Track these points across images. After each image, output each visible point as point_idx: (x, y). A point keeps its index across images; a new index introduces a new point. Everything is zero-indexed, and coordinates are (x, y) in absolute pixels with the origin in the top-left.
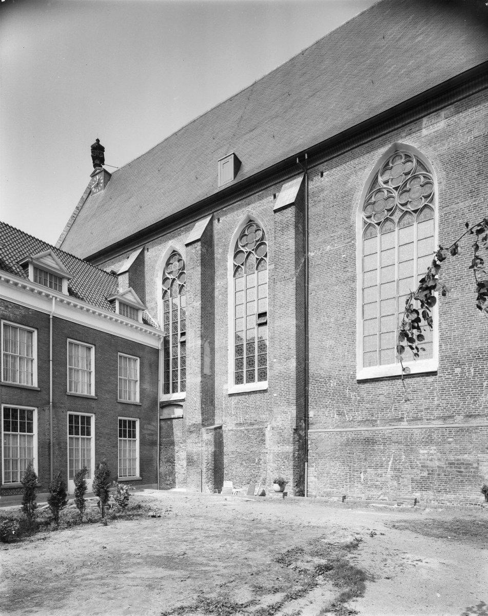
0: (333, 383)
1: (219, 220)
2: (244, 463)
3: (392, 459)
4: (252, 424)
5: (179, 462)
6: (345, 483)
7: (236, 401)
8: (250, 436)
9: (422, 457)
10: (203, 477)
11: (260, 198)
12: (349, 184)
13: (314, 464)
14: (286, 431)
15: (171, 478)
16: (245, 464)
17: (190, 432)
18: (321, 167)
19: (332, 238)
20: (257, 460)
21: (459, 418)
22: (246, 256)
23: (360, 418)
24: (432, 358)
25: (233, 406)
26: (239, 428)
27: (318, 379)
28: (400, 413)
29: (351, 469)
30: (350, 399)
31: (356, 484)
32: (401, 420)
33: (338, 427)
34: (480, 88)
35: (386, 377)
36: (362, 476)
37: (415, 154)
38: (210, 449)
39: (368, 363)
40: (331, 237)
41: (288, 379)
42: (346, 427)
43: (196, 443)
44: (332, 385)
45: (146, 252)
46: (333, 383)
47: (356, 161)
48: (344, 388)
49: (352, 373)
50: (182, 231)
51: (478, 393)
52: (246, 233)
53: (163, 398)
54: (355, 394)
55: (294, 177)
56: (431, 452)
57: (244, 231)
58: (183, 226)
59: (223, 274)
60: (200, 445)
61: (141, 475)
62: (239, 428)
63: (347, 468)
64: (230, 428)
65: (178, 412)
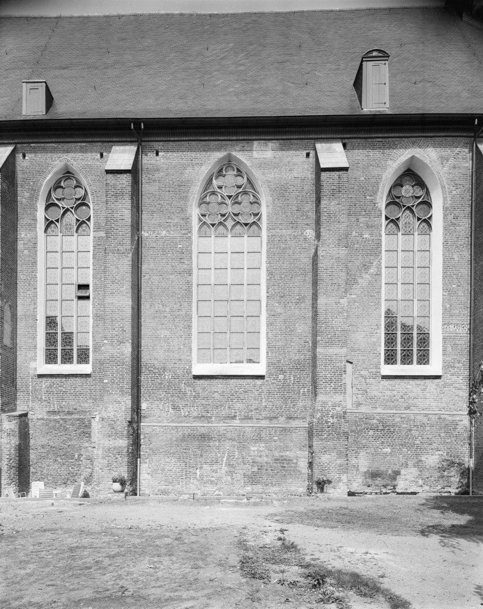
0: (168, 376)
1: (24, 156)
2: (59, 459)
3: (226, 455)
4: (69, 413)
7: (48, 384)
11: (83, 150)
13: (147, 461)
14: (119, 423)
18: (157, 146)
20: (76, 456)
21: (282, 419)
23: (195, 414)
29: (188, 465)
30: (185, 393)
32: (234, 417)
33: (173, 421)
35: (222, 376)
36: (198, 472)
38: (13, 442)
40: (167, 223)
42: (181, 422)
44: (167, 377)
45: (19, 156)
47: (193, 154)
49: (187, 367)
52: (62, 184)
56: (260, 449)
59: (30, 225)
64: (40, 417)
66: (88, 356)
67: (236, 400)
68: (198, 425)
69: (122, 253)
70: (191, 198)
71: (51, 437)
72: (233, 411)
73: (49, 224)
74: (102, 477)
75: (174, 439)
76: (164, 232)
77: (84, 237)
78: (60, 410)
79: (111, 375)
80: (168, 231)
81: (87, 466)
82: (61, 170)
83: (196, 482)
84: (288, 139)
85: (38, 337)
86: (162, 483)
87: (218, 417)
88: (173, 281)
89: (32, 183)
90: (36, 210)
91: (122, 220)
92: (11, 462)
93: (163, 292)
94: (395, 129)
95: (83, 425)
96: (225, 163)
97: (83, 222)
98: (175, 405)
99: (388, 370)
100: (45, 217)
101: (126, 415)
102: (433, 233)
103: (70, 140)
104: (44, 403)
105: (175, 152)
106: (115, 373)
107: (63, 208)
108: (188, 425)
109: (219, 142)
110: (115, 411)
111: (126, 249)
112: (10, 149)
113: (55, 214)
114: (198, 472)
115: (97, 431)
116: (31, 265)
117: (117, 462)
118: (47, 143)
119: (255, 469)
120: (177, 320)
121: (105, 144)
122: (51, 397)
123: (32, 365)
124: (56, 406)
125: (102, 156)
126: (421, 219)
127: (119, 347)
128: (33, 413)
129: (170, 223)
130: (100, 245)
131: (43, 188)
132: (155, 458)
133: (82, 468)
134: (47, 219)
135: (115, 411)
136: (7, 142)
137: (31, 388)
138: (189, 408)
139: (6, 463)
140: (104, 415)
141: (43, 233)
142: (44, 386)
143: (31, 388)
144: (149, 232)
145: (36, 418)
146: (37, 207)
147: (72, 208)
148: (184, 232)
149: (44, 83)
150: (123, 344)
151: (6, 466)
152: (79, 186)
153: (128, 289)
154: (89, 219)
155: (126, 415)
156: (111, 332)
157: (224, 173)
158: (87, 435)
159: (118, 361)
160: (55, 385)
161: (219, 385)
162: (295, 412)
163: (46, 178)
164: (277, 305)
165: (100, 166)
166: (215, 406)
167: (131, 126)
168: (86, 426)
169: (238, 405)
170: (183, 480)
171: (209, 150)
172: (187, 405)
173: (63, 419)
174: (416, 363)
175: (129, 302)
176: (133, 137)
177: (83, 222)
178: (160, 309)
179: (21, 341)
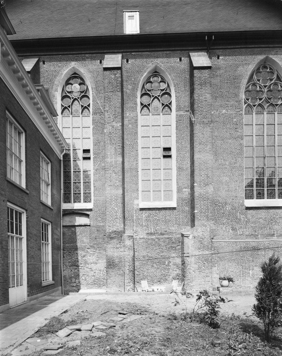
0: (228, 208)
1: (127, 61)
2: (155, 265)
4: (162, 234)
5: (87, 265)
6: (239, 278)
7: (147, 215)
8: (161, 243)
10: (126, 278)
11: (168, 56)
12: (239, 72)
13: (216, 265)
14: (205, 239)
15: (77, 281)
17: (111, 238)
18: (218, 52)
19: (227, 105)
20: (167, 263)
22: (152, 99)
23: (247, 233)
24: (172, 200)
25: (144, 219)
26: (150, 237)
27: (217, 203)
28: (272, 231)
29: (244, 268)
30: (240, 220)
31: (247, 278)
32: (273, 235)
33: (232, 238)
36: (251, 272)
37: (276, 69)
39: (145, 199)
40: (226, 104)
41: (207, 200)
42: (238, 239)
43: (117, 248)
44: (227, 209)
45: (41, 63)
46: (228, 208)
47: (243, 57)
48: (236, 212)
49: (241, 202)
50: (88, 58)
51: (167, 222)
52: (151, 80)
53: (65, 206)
54: (243, 216)
57: (149, 78)
58: (89, 53)
59: (132, 107)
60: (122, 250)
61: (53, 279)
62: (150, 237)
63: (241, 267)
64: (142, 237)
65: (80, 220)
67: (274, 223)
68: (249, 240)
69: (206, 124)
70: (242, 87)
71: (149, 251)
72: (272, 231)
73: (64, 109)
77: (167, 116)
79: (199, 207)
80: (227, 110)
81: (174, 270)
83: (249, 279)
85: (139, 183)
87: (262, 235)
88: (230, 144)
89: (133, 79)
90: (137, 98)
91: (206, 101)
92: (130, 268)
93: (224, 151)
95: (171, 242)
96: (262, 64)
97: (86, 107)
98: (234, 227)
99: (249, 203)
100: (62, 104)
102: (172, 113)
104: (144, 228)
105: (230, 56)
106: (202, 206)
107: (73, 98)
109: (261, 49)
110: (203, 232)
111: (209, 121)
112: (36, 59)
113: (68, 102)
114: (251, 272)
116: (133, 135)
117: (204, 266)
121: (183, 52)
122: (149, 223)
123: (136, 202)
124: (152, 229)
125: (180, 60)
126: (70, 105)
128: (137, 234)
129: (228, 104)
130: (181, 120)
131: (141, 82)
132: (221, 263)
133: (171, 271)
134: (62, 106)
135: (203, 232)
136: (116, 51)
137: (135, 218)
138: (243, 229)
139: (127, 268)
140: (196, 234)
141: (61, 115)
142: (144, 216)
144: (214, 111)
145: (139, 238)
146: (137, 95)
147: (78, 98)
148: (237, 110)
149: (138, 12)
150: (208, 186)
151: (127, 271)
152: (163, 81)
153: (210, 148)
154: (89, 105)
155: (211, 234)
156: (199, 178)
157: (261, 70)
158: (174, 249)
159: (205, 198)
160: (151, 215)
161: (263, 213)
163: (143, 76)
165: (180, 67)
166: (260, 228)
167: (206, 37)
170: (241, 278)
171: (254, 54)
172: (241, 227)
174: (171, 202)
177: (66, 108)
178: (222, 163)
179: (127, 186)
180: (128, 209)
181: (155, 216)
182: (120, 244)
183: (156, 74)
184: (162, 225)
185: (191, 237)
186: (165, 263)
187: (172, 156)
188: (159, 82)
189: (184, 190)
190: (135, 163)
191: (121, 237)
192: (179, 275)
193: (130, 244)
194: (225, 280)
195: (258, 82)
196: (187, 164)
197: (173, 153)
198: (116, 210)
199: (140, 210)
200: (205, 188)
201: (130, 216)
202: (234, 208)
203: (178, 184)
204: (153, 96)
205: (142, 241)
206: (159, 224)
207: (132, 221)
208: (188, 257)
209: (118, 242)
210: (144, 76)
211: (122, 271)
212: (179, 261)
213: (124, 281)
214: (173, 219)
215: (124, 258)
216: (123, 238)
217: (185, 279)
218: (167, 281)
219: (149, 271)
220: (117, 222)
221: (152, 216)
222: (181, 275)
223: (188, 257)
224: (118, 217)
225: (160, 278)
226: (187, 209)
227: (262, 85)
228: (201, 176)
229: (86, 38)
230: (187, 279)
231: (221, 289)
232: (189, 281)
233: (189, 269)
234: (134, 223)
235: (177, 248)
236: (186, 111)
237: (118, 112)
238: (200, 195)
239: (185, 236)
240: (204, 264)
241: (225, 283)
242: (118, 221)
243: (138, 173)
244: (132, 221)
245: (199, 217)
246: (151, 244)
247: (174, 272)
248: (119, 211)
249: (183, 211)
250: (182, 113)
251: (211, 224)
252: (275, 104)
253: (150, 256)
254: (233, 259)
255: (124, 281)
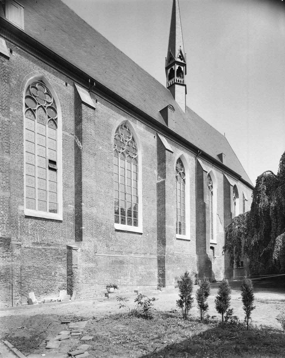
0: (104, 228)
3: (130, 271)
4: (48, 245)
8: (47, 254)
9: (140, 270)
14: (91, 253)
16: (42, 277)
20: (53, 274)
21: (148, 254)
23: (116, 250)
26: (36, 247)
29: (115, 277)
30: (111, 239)
33: (106, 253)
34: (26, 49)
35: (127, 231)
39: (31, 206)
41: (92, 220)
44: (103, 229)
47: (113, 112)
51: (54, 233)
55: (79, 85)
56: (142, 268)
57: (35, 83)
60: (10, 259)
62: (36, 247)
66: (39, 206)
69: (91, 154)
74: (82, 286)
75: (108, 263)
76: (101, 148)
78: (42, 242)
80: (103, 147)
81: (60, 280)
82: (39, 78)
84: (148, 126)
86: (103, 287)
92: (19, 279)
94: (67, 72)
95: (58, 253)
101: (95, 249)
102: (58, 130)
103: (125, 111)
104: (30, 237)
108: (114, 255)
115: (79, 258)
118: (30, 53)
119: (141, 278)
120: (107, 198)
122: (35, 233)
123: (20, 208)
125: (66, 84)
127: (90, 209)
137: (19, 224)
139: (16, 280)
142: (30, 224)
143: (19, 224)
151: (16, 282)
152: (48, 93)
160: (38, 225)
162: (152, 251)
164: (146, 201)
168: (59, 254)
169: (133, 247)
173: (44, 249)
175: (85, 182)
176: (88, 86)
180: (11, 214)
181: (42, 226)
182: (7, 253)
183: (42, 84)
184: (48, 236)
185: (79, 251)
186: (52, 273)
187: (58, 171)
188: (45, 93)
189: (69, 206)
190: (19, 166)
191: (9, 245)
192: (64, 285)
193: (19, 253)
194: (112, 287)
195: (122, 136)
196: (72, 182)
197: (59, 166)
198: (2, 214)
199: (25, 218)
200: (90, 209)
201: (13, 222)
202: (107, 229)
203: (64, 199)
204: (39, 104)
205: (27, 250)
206: (45, 234)
207: (15, 228)
208: (76, 268)
209: (5, 250)
210: (31, 79)
211: (10, 283)
212: (64, 271)
213: (12, 294)
214: (60, 231)
215: (12, 268)
216: (10, 247)
217: (73, 288)
218: (53, 292)
219: (35, 282)
220: (4, 228)
221: (39, 226)
222: (66, 285)
223: (76, 268)
224: (5, 222)
225: (46, 289)
226: (72, 223)
227: (124, 139)
228: (88, 198)
229: (6, 22)
230: (75, 288)
231: (109, 295)
232: (78, 290)
233: (77, 279)
234: (18, 230)
235: (63, 259)
236: (71, 134)
237: (6, 104)
238: (86, 214)
239: (74, 249)
240: (90, 274)
241: (112, 289)
242: (5, 227)
243: (23, 178)
244: (15, 228)
245: (86, 233)
246: (37, 254)
247: (60, 282)
248: (6, 216)
249: (68, 225)
250: (67, 134)
251: (95, 240)
252: (33, 110)
253: (36, 267)
254: (107, 270)
255: (12, 294)
